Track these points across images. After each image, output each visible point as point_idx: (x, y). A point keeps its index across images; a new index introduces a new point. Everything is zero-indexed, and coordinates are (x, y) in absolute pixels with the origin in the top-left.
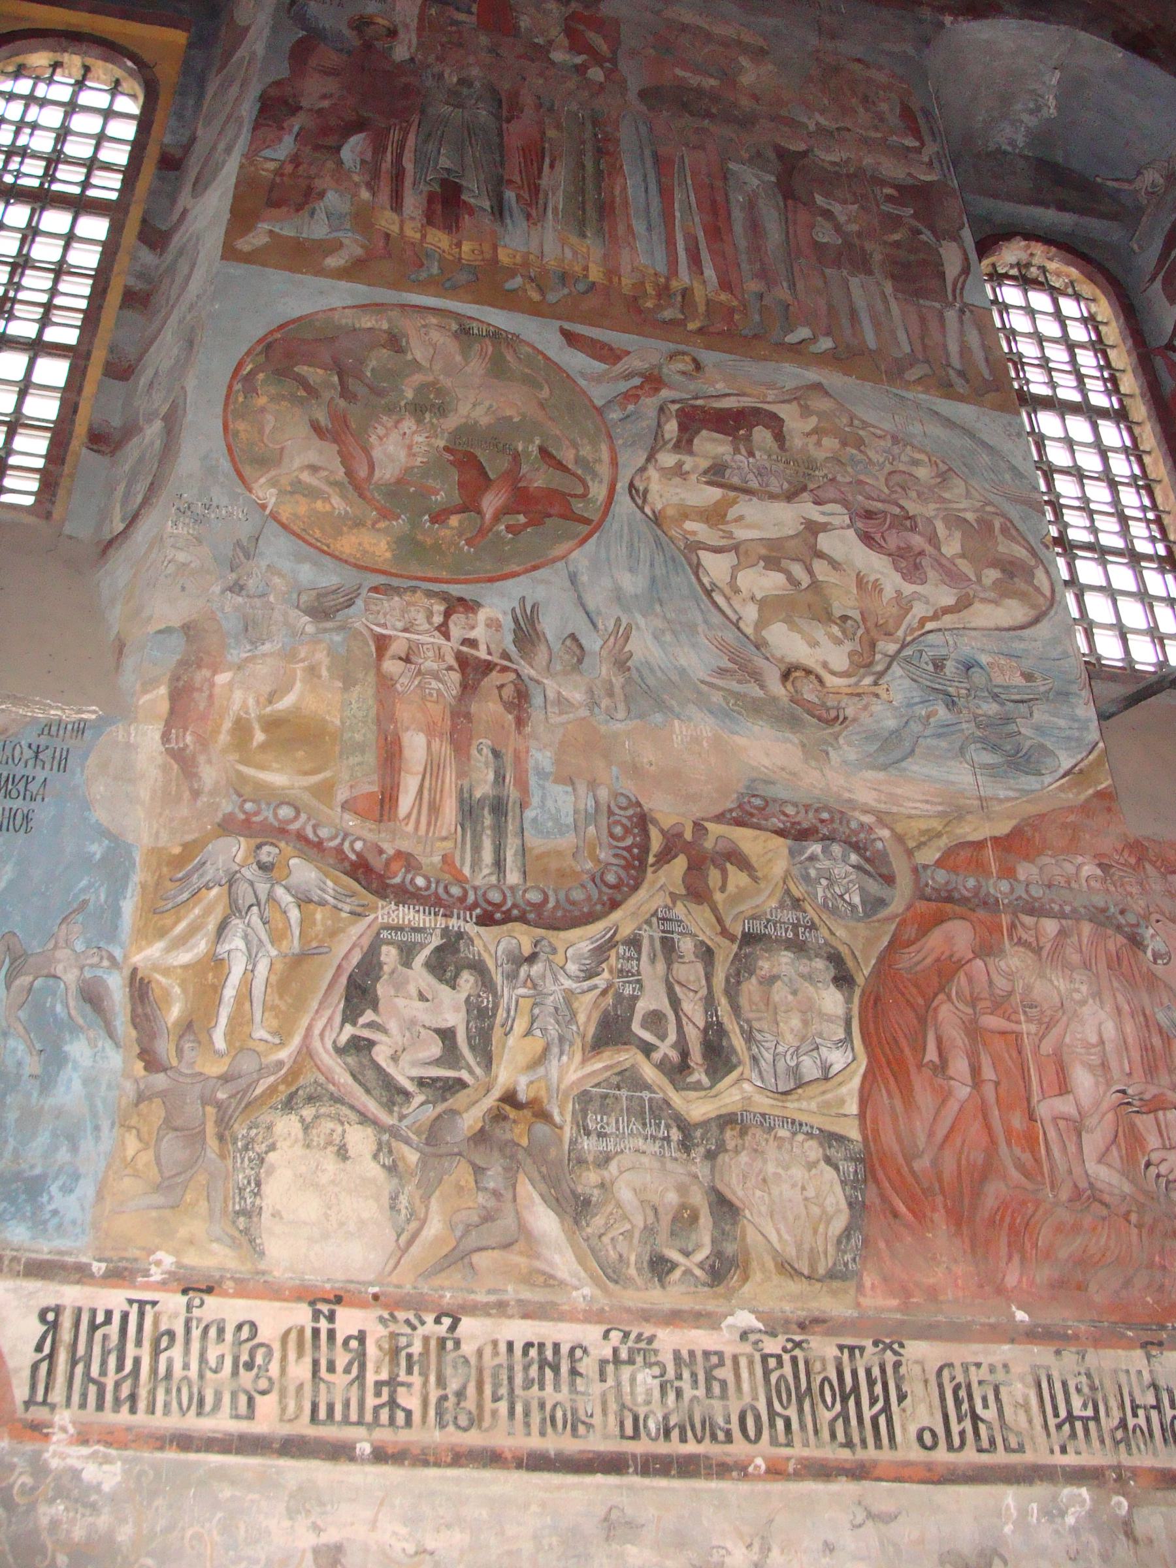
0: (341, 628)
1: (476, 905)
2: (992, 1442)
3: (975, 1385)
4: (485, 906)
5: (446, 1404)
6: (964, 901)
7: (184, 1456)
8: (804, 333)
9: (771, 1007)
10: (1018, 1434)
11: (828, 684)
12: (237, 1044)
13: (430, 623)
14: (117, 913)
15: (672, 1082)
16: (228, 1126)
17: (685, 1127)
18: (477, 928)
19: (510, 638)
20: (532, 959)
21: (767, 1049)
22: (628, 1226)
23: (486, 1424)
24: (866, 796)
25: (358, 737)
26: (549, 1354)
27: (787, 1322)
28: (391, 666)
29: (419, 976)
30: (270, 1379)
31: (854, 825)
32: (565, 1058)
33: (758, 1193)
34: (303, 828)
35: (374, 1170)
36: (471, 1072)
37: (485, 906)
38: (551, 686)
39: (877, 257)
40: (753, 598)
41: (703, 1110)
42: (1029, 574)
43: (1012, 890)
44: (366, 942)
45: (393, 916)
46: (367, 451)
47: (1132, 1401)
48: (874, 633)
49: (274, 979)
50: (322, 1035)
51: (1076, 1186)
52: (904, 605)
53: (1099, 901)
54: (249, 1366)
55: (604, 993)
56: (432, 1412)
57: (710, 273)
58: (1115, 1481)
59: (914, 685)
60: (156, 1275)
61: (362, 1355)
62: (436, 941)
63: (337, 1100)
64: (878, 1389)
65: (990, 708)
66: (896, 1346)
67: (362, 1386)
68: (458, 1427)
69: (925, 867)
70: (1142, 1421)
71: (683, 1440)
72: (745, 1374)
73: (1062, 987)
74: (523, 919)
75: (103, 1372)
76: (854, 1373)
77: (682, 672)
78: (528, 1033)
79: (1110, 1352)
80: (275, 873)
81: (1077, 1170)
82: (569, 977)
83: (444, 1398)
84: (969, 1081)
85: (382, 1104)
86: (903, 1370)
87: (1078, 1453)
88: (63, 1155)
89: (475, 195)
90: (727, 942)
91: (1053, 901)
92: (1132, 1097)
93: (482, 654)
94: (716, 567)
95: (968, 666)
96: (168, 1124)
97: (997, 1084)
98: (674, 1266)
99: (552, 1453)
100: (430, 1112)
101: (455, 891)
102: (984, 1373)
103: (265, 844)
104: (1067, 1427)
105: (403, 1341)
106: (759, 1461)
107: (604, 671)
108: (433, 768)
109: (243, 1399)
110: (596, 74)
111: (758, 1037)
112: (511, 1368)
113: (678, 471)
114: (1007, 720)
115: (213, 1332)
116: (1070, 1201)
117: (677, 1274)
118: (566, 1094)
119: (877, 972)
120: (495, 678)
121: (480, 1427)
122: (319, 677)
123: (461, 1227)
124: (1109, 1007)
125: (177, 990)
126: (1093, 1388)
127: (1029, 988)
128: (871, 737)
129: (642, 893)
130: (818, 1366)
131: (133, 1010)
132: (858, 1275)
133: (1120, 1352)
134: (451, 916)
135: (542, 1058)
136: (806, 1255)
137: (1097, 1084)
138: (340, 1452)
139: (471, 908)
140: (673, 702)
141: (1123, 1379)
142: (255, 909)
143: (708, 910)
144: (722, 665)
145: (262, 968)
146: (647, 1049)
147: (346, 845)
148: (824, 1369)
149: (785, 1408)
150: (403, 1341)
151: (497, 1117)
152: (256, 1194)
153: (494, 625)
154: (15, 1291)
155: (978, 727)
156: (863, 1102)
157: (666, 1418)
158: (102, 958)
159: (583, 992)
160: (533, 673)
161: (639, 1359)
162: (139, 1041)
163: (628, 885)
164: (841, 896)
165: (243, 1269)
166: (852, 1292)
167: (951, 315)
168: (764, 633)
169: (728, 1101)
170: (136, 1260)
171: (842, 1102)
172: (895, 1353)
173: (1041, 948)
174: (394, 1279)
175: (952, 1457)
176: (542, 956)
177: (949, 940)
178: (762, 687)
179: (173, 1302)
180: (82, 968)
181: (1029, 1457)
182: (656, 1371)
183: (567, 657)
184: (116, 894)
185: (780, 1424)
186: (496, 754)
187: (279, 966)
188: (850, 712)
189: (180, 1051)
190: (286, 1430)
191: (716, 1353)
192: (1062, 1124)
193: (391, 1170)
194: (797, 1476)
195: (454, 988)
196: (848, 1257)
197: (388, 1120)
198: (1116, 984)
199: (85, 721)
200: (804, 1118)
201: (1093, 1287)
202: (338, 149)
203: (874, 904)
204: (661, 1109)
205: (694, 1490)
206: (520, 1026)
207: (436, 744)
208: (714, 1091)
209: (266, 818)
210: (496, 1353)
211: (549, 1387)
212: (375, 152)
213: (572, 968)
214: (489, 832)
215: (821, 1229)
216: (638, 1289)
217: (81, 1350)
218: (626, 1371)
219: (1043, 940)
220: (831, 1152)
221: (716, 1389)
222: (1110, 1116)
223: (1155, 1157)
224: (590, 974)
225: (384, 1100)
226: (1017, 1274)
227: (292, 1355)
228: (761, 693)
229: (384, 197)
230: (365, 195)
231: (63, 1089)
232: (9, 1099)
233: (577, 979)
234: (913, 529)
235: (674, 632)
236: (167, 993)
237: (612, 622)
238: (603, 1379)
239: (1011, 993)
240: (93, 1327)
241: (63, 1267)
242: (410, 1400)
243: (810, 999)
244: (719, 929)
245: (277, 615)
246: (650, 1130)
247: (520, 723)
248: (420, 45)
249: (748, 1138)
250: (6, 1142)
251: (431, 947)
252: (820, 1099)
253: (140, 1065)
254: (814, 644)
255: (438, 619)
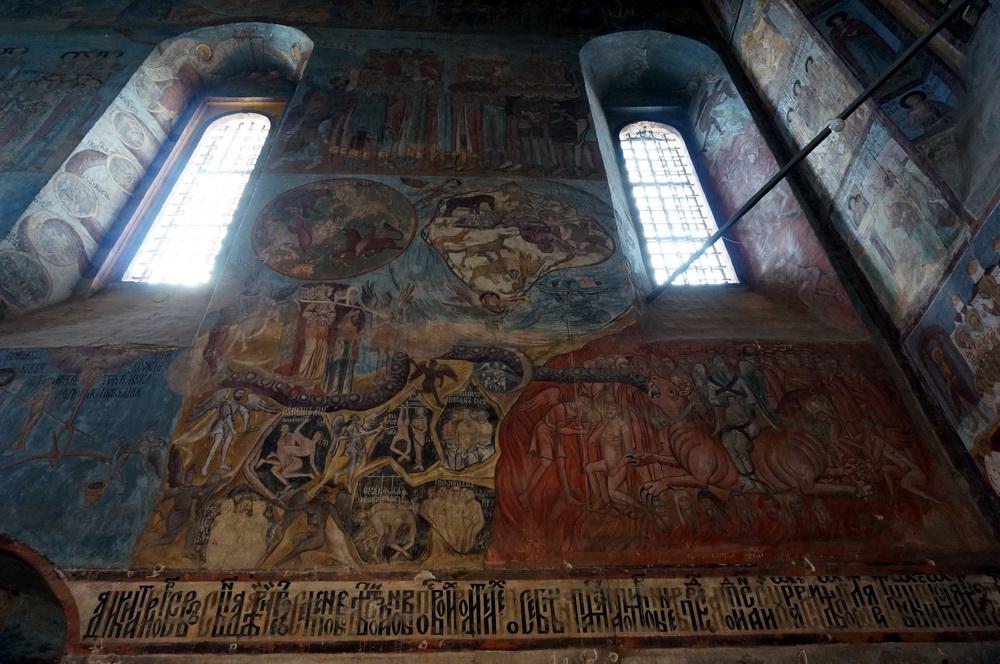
0: (289, 302)
1: (326, 404)
2: (547, 628)
3: (540, 600)
6: (557, 379)
7: (149, 656)
8: (508, 164)
14: (170, 423)
17: (409, 488)
23: (293, 632)
25: (287, 343)
26: (329, 597)
27: (447, 574)
28: (306, 314)
29: (297, 435)
31: (506, 353)
35: (262, 519)
36: (315, 475)
38: (375, 313)
39: (546, 130)
40: (471, 268)
42: (603, 242)
43: (581, 372)
44: (275, 424)
46: (310, 234)
47: (625, 604)
50: (250, 465)
51: (602, 501)
52: (541, 262)
57: (470, 148)
60: (155, 574)
61: (242, 602)
63: (251, 491)
64: (490, 604)
67: (239, 618)
69: (539, 367)
70: (630, 614)
74: (347, 408)
75: (122, 620)
76: (478, 597)
77: (435, 301)
81: (604, 495)
85: (271, 490)
86: (503, 595)
88: (126, 526)
89: (372, 135)
93: (347, 305)
94: (456, 258)
95: (569, 283)
100: (293, 492)
101: (319, 399)
104: (588, 619)
106: (425, 642)
108: (318, 351)
109: (183, 627)
110: (431, 83)
111: (449, 446)
112: (310, 604)
113: (444, 224)
115: (176, 598)
120: (351, 313)
124: (626, 418)
125: (190, 452)
126: (603, 598)
127: (585, 414)
128: (519, 316)
129: (403, 392)
132: (485, 551)
133: (621, 580)
135: (347, 465)
137: (617, 454)
138: (222, 649)
141: (621, 593)
145: (229, 439)
146: (396, 457)
148: (463, 595)
151: (323, 492)
153: (354, 293)
156: (497, 470)
157: (381, 624)
160: (368, 310)
161: (372, 597)
167: (578, 147)
174: (263, 567)
175: (525, 636)
179: (161, 586)
180: (151, 448)
181: (566, 634)
182: (379, 601)
185: (438, 623)
186: (346, 342)
187: (236, 437)
190: (200, 640)
193: (271, 519)
194: (443, 649)
200: (467, 480)
202: (317, 127)
203: (511, 385)
205: (390, 658)
206: (339, 452)
210: (304, 598)
212: (332, 127)
213: (366, 425)
221: (408, 609)
222: (624, 468)
223: (646, 485)
229: (333, 141)
230: (326, 141)
234: (549, 231)
235: (433, 286)
240: (122, 599)
242: (259, 623)
247: (359, 330)
248: (358, 85)
249: (439, 492)
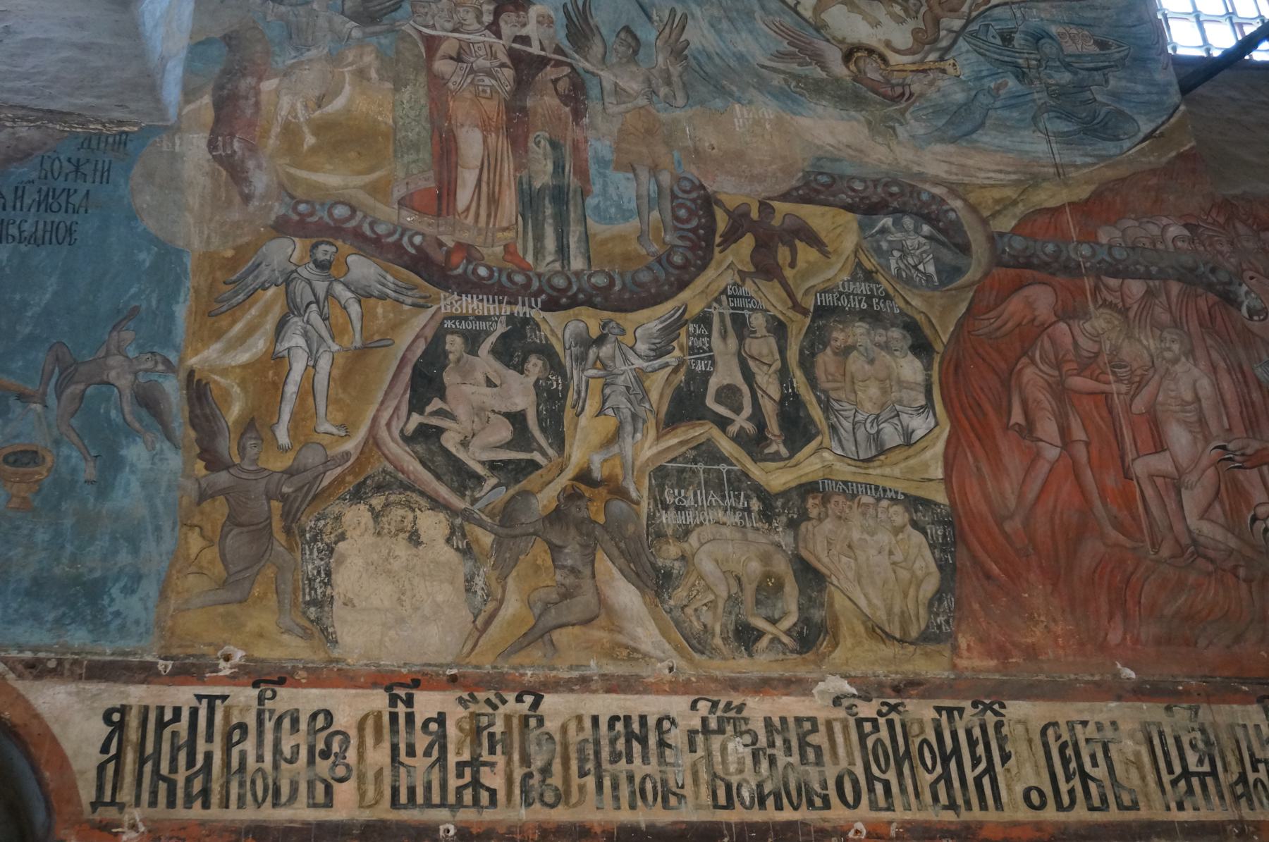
0: (392, 30)
2: (1104, 799)
3: (1082, 744)
4: (550, 291)
5: (531, 782)
6: (1044, 266)
9: (848, 379)
10: (1131, 791)
11: (892, 62)
12: (302, 438)
13: (480, 22)
14: (170, 317)
15: (750, 454)
16: (296, 519)
18: (543, 314)
19: (562, 34)
20: (600, 341)
21: (846, 418)
22: (711, 597)
24: (935, 169)
26: (636, 727)
27: (881, 685)
29: (485, 362)
30: (347, 766)
31: (924, 197)
32: (639, 435)
33: (844, 559)
34: (360, 226)
35: (448, 554)
36: (544, 454)
37: (550, 291)
38: (607, 77)
41: (783, 480)
43: (1094, 254)
44: (429, 333)
45: (457, 306)
47: (1252, 755)
48: (938, 10)
49: (336, 372)
50: (388, 425)
51: (1177, 541)
53: (1188, 260)
54: (325, 754)
55: (676, 370)
56: (517, 791)
58: (1238, 836)
59: (982, 59)
60: (225, 669)
61: (442, 737)
62: (501, 328)
63: (407, 487)
64: (980, 750)
65: (1066, 77)
66: (996, 707)
67: (444, 768)
68: (545, 804)
69: (1002, 235)
71: (779, 807)
72: (840, 739)
73: (1152, 347)
74: (589, 303)
75: (174, 768)
76: (954, 735)
77: (741, 58)
78: (600, 413)
79: (1225, 708)
80: (333, 271)
81: (1178, 527)
82: (640, 356)
83: (529, 775)
84: (1058, 441)
86: (1005, 730)
87: (1196, 809)
88: (124, 558)
90: (800, 317)
91: (1138, 263)
92: (1233, 452)
93: (535, 50)
95: (1037, 37)
96: (233, 520)
97: (1087, 444)
98: (761, 634)
99: (643, 826)
100: (503, 494)
102: (1091, 730)
103: (322, 243)
104: (1182, 783)
105: (484, 721)
107: (661, 59)
108: (490, 163)
109: (320, 788)
111: (836, 406)
112: (597, 743)
114: (1081, 87)
115: (286, 723)
116: (1173, 557)
117: (764, 642)
118: (641, 470)
119: (955, 336)
120: (550, 73)
121: (567, 803)
122: (369, 80)
123: (539, 605)
124: (1203, 364)
125: (236, 390)
126: (1208, 743)
127: (1116, 349)
128: (938, 111)
129: (710, 273)
130: (915, 729)
131: (191, 412)
132: (952, 636)
134: (516, 303)
135: (615, 437)
136: (897, 619)
139: (536, 295)
140: (734, 89)
141: (1240, 733)
142: (314, 307)
143: (779, 286)
144: (782, 49)
145: (324, 363)
146: (723, 423)
147: (405, 240)
148: (922, 731)
149: (884, 772)
150: (484, 721)
151: (571, 496)
152: (328, 584)
153: (544, 20)
154: (78, 693)
155: (1050, 95)
157: (760, 786)
158: (156, 363)
159: (655, 371)
160: (588, 66)
161: (729, 729)
162: (199, 441)
163: (695, 266)
164: (915, 267)
165: (316, 658)
166: (947, 653)
168: (823, 16)
169: (808, 470)
170: (203, 656)
171: (926, 466)
172: (996, 713)
173: (1128, 309)
175: (1062, 816)
176: (612, 338)
177: (1030, 305)
178: (823, 68)
180: (136, 374)
182: (748, 739)
183: (622, 49)
184: (169, 298)
185: (879, 787)
186: (554, 145)
187: (340, 361)
188: (916, 88)
189: (242, 450)
191: (809, 719)
192: (1159, 481)
195: (522, 373)
196: (941, 619)
197: (459, 504)
198: (1209, 342)
199: (127, 133)
200: (888, 484)
201: (1202, 642)
203: (949, 273)
204: (740, 481)
206: (592, 406)
207: (492, 138)
208: (793, 461)
209: (321, 218)
210: (580, 728)
211: (637, 760)
213: (642, 347)
214: (550, 221)
215: (912, 592)
216: (724, 659)
217: (149, 748)
218: (716, 741)
219: (1129, 301)
220: (918, 516)
221: (811, 755)
222: (1211, 472)
224: (660, 352)
225: (456, 484)
226: (1120, 633)
227: (370, 741)
228: (824, 75)
231: (121, 492)
232: (64, 506)
233: (648, 358)
235: (731, 20)
236: (226, 394)
237: (667, 13)
238: (693, 750)
239: (1097, 355)
240: (161, 725)
241: (128, 667)
242: (493, 779)
243: (888, 367)
244: (790, 304)
245: (322, 22)
246: (730, 502)
247: (578, 115)
249: (831, 506)
250: (63, 547)
251: (497, 334)
252: (903, 465)
253: (200, 465)
254: (876, 24)
255: (487, 19)
